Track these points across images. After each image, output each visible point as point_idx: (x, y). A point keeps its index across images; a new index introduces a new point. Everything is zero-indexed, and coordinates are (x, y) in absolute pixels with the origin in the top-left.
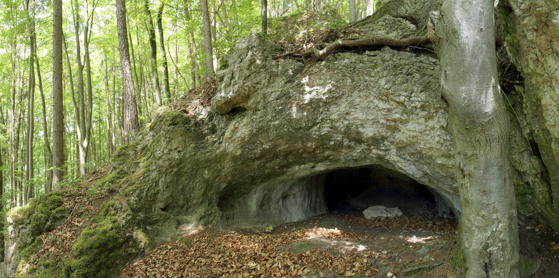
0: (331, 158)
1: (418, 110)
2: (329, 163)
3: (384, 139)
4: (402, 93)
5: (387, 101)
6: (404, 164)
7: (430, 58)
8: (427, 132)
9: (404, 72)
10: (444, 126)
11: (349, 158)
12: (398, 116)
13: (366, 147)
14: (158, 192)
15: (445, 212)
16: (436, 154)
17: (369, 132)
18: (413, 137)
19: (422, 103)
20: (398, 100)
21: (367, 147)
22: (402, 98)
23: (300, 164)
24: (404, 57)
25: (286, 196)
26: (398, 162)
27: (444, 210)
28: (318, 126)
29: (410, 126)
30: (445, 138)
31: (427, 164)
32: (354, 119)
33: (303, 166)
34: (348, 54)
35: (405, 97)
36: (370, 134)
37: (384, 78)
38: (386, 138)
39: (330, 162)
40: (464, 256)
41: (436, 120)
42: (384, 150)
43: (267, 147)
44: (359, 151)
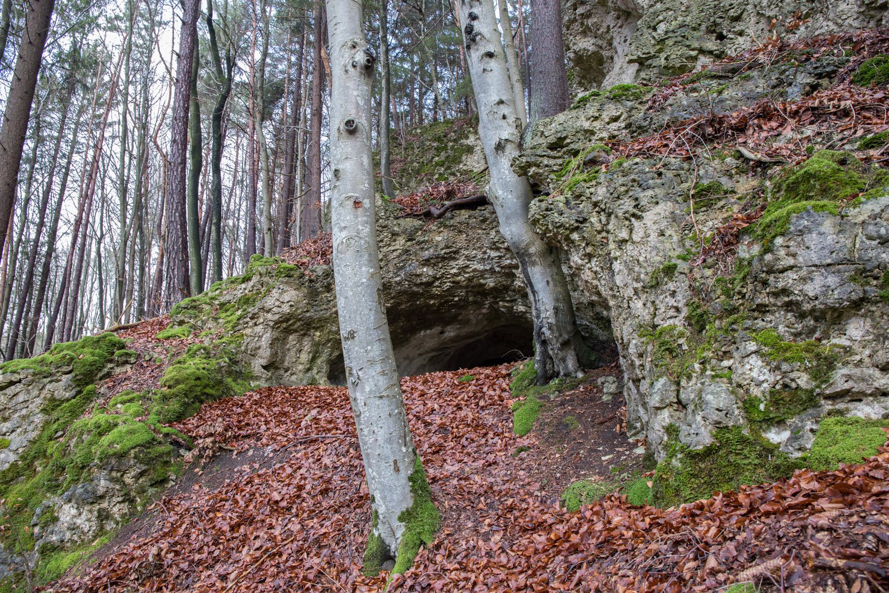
12: (509, 261)
14: (259, 348)
17: (490, 283)
33: (428, 331)
34: (463, 211)
36: (492, 285)
40: (454, 18)
44: (487, 306)
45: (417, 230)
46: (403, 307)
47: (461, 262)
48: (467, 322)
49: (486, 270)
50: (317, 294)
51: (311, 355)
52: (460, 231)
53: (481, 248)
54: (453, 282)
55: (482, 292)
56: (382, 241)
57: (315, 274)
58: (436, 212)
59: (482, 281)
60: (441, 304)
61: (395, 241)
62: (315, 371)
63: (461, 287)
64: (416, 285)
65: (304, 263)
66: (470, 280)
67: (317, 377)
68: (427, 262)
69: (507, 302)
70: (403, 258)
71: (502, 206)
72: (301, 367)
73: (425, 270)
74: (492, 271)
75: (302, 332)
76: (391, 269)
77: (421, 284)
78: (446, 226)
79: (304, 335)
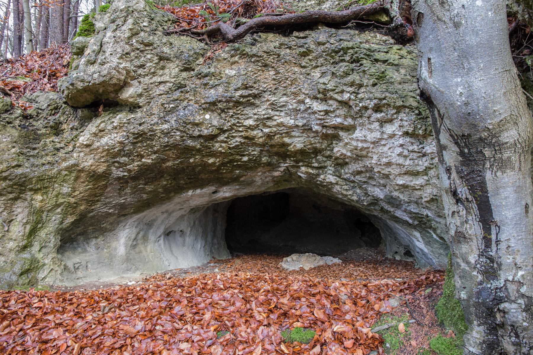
0: (242, 179)
1: (370, 112)
2: (237, 187)
3: (316, 152)
4: (345, 88)
5: (325, 100)
6: (346, 187)
7: (378, 35)
8: (383, 142)
9: (347, 58)
10: (410, 131)
11: (267, 180)
12: (339, 120)
13: (292, 163)
15: (396, 253)
16: (394, 171)
17: (297, 142)
18: (362, 149)
19: (375, 101)
20: (339, 98)
21: (295, 164)
22: (346, 96)
23: (195, 187)
24: (344, 38)
25: (170, 232)
26: (337, 184)
27: (395, 249)
29: (358, 134)
30: (411, 148)
31: (379, 185)
32: (278, 125)
33: (198, 191)
34: (271, 36)
35: (351, 94)
36: (299, 146)
37: (319, 69)
39: (239, 185)
41: (397, 124)
43: (149, 161)
44: (282, 169)
45: (197, 55)
46: (169, 164)
47: (262, 111)
48: (250, 183)
49: (297, 126)
50: (37, 138)
51: (28, 227)
52: (266, 66)
53: (295, 94)
54: (246, 138)
55: (282, 152)
56: (142, 66)
57: (34, 105)
58: (229, 30)
59: (287, 140)
60: (223, 164)
61: (163, 68)
62: (36, 247)
63: (255, 144)
64: (192, 137)
65: (18, 87)
66: (269, 136)
67: (39, 256)
68: (211, 106)
69: (313, 168)
70: (177, 94)
71: (457, 25)
72: (11, 245)
73: (207, 116)
74: (307, 129)
75: (11, 196)
76: (155, 111)
77: (200, 136)
78: (243, 55)
79: (16, 199)
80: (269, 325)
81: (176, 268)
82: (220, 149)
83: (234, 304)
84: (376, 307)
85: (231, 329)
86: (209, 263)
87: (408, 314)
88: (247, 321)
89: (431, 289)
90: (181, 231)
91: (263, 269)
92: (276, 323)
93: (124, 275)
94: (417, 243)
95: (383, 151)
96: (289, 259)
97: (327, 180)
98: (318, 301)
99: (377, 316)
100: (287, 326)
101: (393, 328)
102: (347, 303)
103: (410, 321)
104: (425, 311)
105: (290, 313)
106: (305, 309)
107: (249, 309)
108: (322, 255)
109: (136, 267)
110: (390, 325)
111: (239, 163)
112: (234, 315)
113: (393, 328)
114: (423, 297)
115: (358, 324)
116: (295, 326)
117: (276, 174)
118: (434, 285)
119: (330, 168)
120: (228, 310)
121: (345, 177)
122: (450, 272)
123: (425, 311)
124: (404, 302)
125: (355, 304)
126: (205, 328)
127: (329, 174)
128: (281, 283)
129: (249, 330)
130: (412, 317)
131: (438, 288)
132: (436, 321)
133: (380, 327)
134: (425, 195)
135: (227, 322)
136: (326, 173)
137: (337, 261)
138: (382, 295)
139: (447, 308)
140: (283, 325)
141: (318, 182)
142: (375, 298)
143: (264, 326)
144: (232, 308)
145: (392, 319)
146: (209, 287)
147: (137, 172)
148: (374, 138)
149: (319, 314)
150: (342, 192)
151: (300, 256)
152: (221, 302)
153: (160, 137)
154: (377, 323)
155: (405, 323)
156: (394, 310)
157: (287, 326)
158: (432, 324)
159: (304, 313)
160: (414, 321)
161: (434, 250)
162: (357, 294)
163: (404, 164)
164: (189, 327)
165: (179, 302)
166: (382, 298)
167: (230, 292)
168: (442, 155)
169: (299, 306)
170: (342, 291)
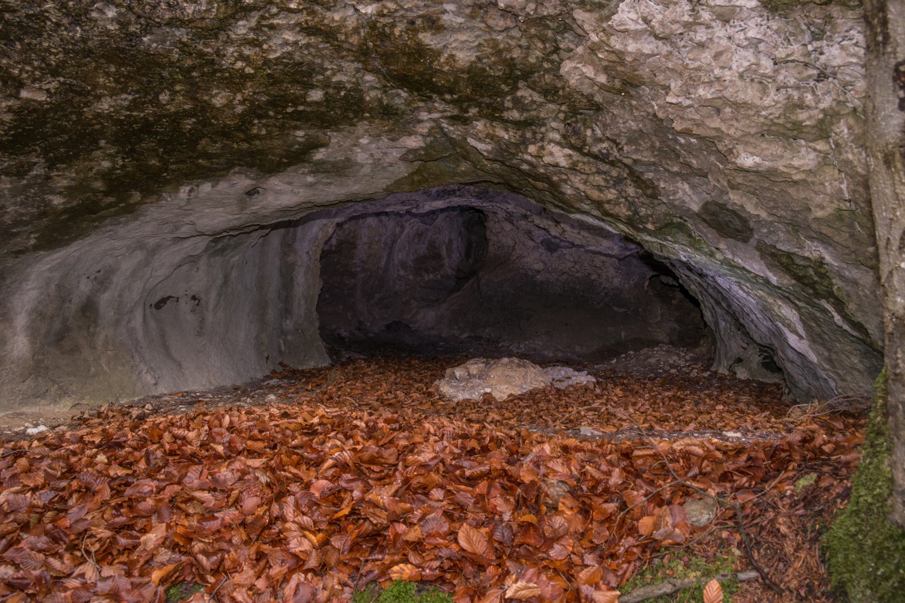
2: (310, 179)
3: (517, 74)
15: (739, 360)
28: (253, 23)
30: (781, 53)
36: (464, 58)
38: (527, 74)
42: (519, 125)
43: (42, 97)
44: (424, 128)
69: (506, 123)
80: (322, 569)
81: (175, 390)
82: (239, 64)
83: (237, 502)
84: (645, 524)
85: (211, 579)
86: (268, 377)
87: (737, 552)
88: (261, 555)
89: (814, 476)
90: (194, 298)
91: (391, 396)
92: (345, 564)
93: (25, 409)
94: (792, 339)
95: (697, 64)
96: (459, 372)
97: (547, 159)
98: (480, 499)
99: (644, 551)
100: (371, 576)
101: (688, 595)
102: (561, 507)
103: (742, 576)
104: (789, 549)
105: (389, 533)
106: (437, 523)
107: (277, 518)
108: (544, 363)
109: (60, 388)
110: (679, 583)
111: (301, 108)
112: (228, 537)
113: (688, 595)
114: (787, 501)
115: (583, 575)
116: (395, 576)
117: (413, 142)
118: (826, 463)
119: (554, 124)
120: (217, 518)
121: (595, 150)
122: (879, 433)
123: (789, 549)
124: (730, 513)
125: (585, 511)
126: (136, 573)
127: (551, 141)
128: (391, 442)
129: (261, 584)
130: (749, 563)
131: (835, 473)
132: (824, 582)
133: (648, 589)
134: (818, 199)
135: (201, 557)
136: (542, 139)
137: (583, 378)
138: (666, 487)
139: (861, 549)
140: (363, 571)
141: (525, 167)
142: (646, 495)
143: (306, 572)
144: (229, 515)
145: (687, 566)
146: (189, 449)
147: (10, 129)
148: (674, 22)
149: (472, 539)
150: (589, 192)
151: (487, 363)
152: (205, 495)
153: (58, 25)
154: (642, 574)
155: (726, 581)
156: (696, 537)
157: (371, 576)
158: (810, 589)
159: (429, 535)
160: (753, 574)
161: (834, 356)
162: (598, 482)
163: (758, 102)
164: (89, 570)
165: (86, 492)
166: (667, 496)
167: (237, 465)
168: (885, 23)
169: (418, 513)
170: (555, 472)
